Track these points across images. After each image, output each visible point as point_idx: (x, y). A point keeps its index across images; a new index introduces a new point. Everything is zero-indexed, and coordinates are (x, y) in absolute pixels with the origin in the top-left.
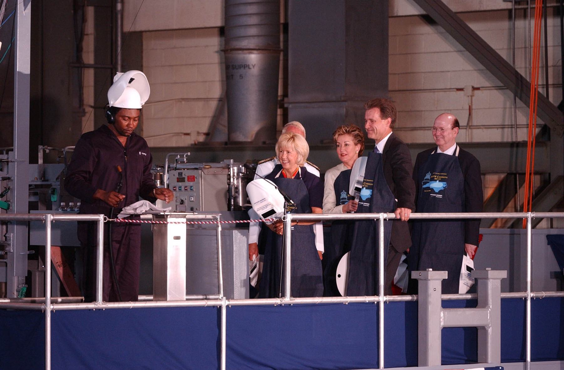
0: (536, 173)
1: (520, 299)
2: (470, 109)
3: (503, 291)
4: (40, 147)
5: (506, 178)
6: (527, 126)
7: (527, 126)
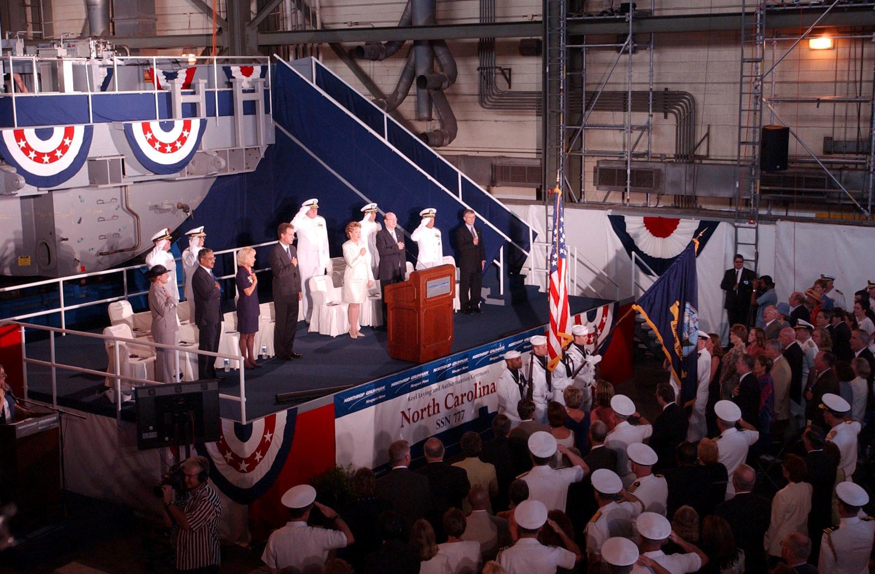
0: (217, 47)
1: (213, 91)
2: (189, 22)
3: (206, 88)
4: (7, 32)
5: (206, 49)
6: (213, 28)
7: (213, 28)
